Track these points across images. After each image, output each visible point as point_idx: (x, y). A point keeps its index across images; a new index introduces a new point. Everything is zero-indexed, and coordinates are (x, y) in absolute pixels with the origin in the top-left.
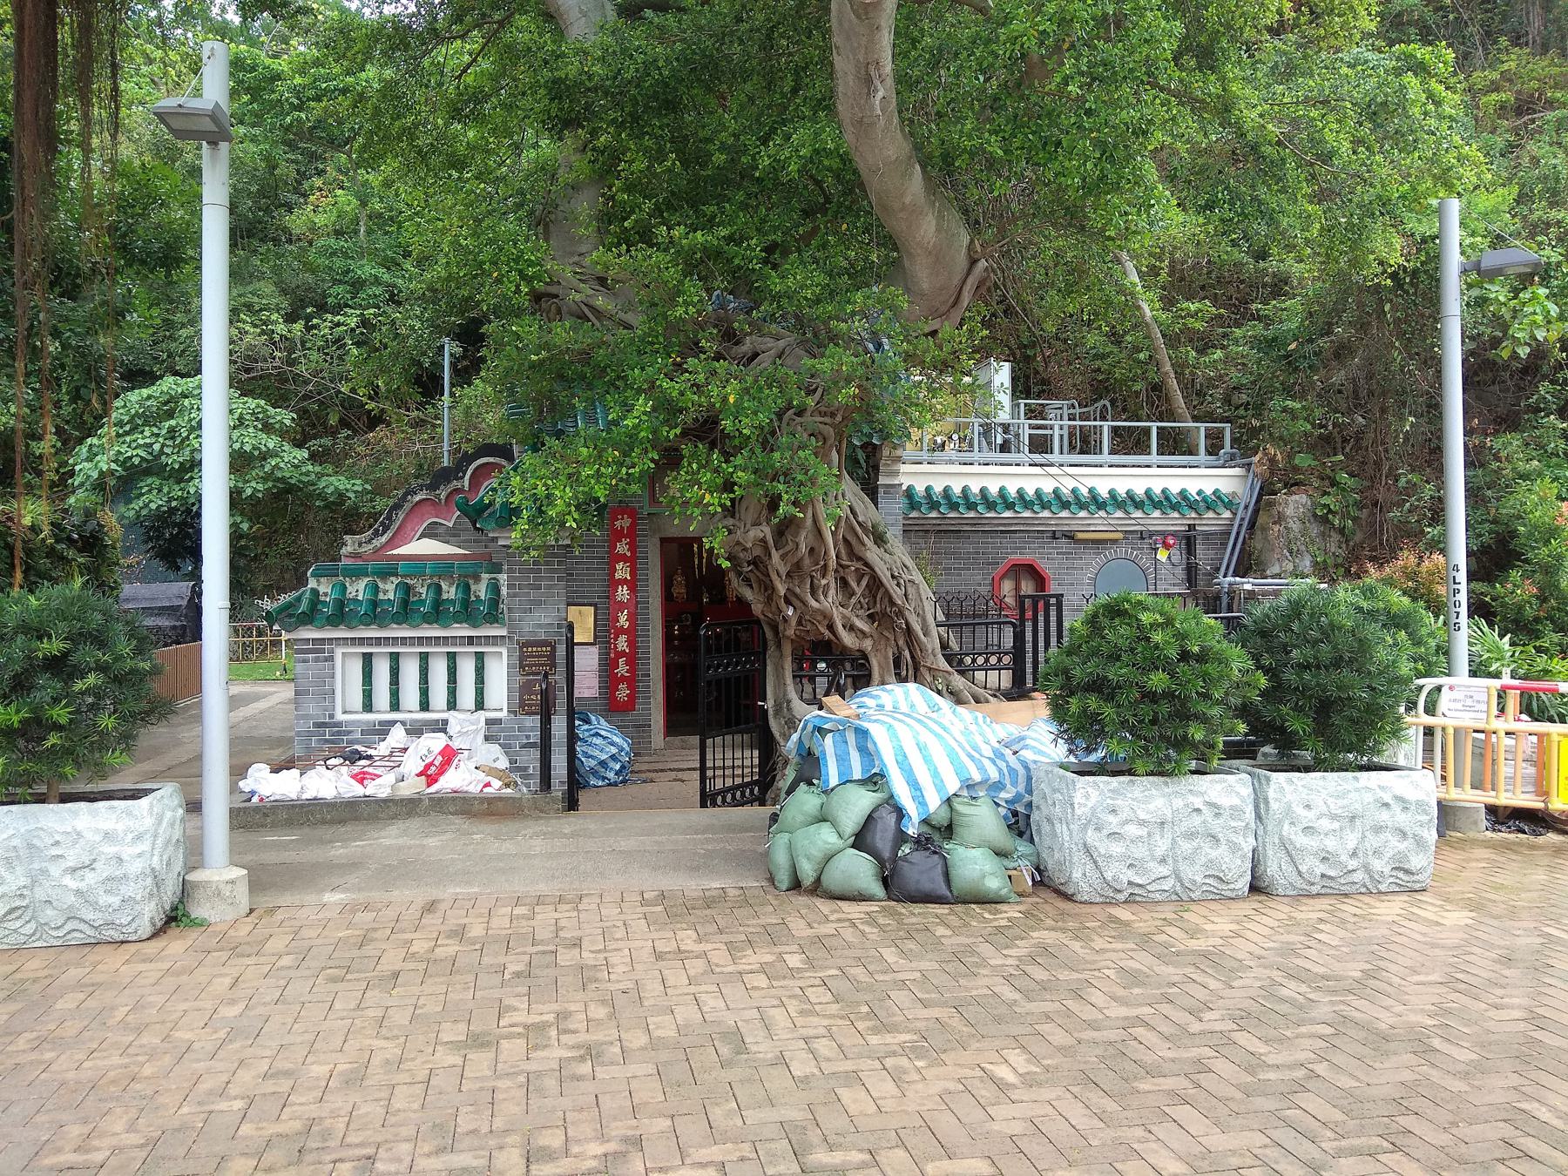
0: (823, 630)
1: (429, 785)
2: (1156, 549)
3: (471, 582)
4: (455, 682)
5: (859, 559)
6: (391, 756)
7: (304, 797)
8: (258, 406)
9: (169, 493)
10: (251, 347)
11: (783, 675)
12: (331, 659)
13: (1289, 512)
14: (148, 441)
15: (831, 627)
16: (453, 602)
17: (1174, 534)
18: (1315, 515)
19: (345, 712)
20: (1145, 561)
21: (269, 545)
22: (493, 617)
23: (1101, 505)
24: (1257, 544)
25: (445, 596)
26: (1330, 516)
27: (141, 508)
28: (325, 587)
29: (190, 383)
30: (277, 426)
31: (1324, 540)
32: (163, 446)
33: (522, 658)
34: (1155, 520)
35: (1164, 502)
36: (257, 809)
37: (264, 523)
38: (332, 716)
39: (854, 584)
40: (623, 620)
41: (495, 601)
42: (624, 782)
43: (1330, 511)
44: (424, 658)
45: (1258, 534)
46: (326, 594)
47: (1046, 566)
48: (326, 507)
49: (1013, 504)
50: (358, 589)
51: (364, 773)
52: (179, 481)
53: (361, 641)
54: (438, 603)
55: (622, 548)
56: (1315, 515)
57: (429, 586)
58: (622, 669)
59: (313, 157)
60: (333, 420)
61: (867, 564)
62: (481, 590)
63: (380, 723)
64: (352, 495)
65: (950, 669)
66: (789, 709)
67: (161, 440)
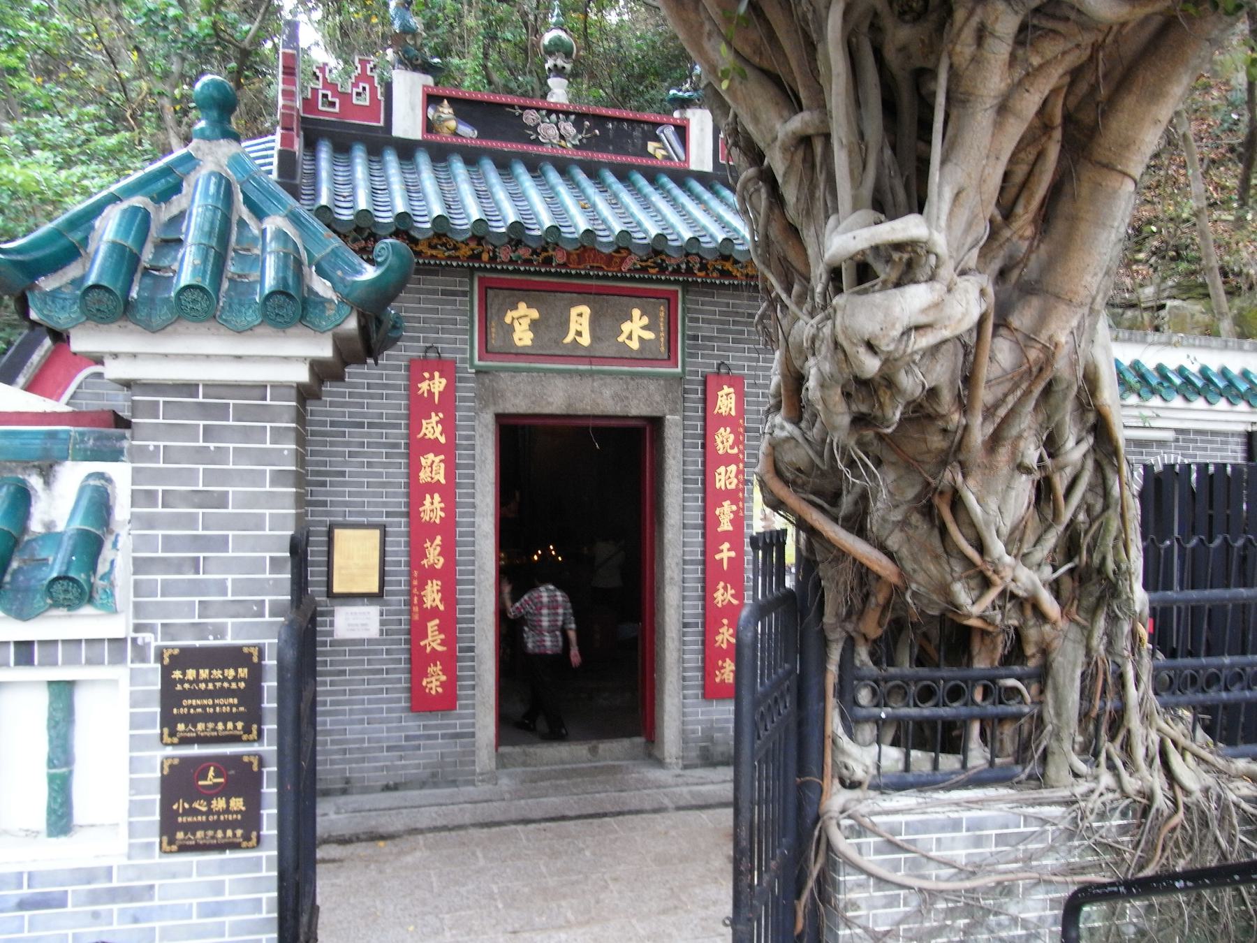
3: (35, 481)
29: (911, 703)
33: (170, 696)
55: (432, 428)
58: (434, 640)
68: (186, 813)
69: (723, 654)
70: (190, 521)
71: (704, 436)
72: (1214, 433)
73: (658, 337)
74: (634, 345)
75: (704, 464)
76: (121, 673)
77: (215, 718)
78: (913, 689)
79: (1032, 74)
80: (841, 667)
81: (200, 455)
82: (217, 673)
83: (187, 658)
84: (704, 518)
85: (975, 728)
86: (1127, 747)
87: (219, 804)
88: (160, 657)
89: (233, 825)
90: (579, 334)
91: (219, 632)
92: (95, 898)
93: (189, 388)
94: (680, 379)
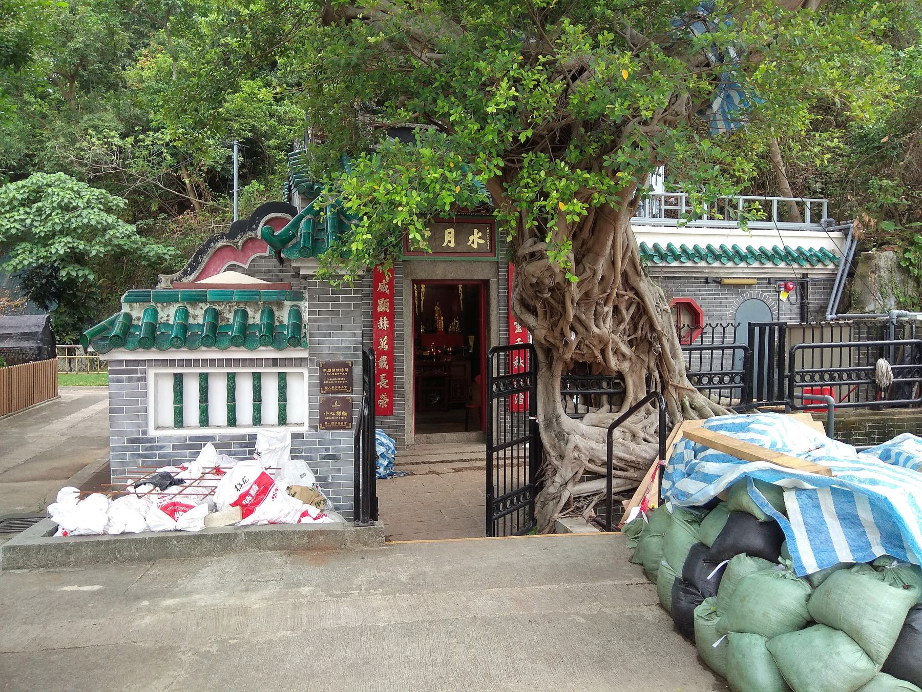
0: (597, 353)
1: (245, 515)
2: (779, 292)
3: (275, 308)
4: (260, 400)
5: (633, 289)
6: (201, 478)
7: (112, 531)
8: (101, 194)
9: (37, 253)
10: (96, 155)
11: (553, 397)
12: (144, 379)
13: (882, 263)
14: (22, 217)
15: (603, 352)
16: (258, 327)
17: (792, 280)
18: (899, 266)
19: (157, 428)
20: (772, 301)
21: (111, 293)
22: (296, 340)
23: (743, 258)
24: (857, 287)
25: (251, 321)
26: (911, 268)
27: (17, 264)
28: (138, 312)
30: (114, 208)
31: (904, 285)
32: (33, 221)
33: (322, 379)
34: (782, 270)
35: (787, 256)
36: (58, 547)
37: (107, 277)
38: (145, 433)
39: (624, 312)
40: (384, 344)
41: (298, 326)
42: (391, 475)
43: (911, 264)
44: (231, 378)
45: (858, 281)
46: (138, 319)
47: (700, 304)
48: (149, 265)
49: (680, 256)
50: (169, 314)
51: (175, 504)
52: (45, 246)
53: (173, 363)
54: (245, 328)
56: (899, 266)
57: (236, 312)
58: (383, 382)
59: (141, 35)
60: (154, 207)
61: (637, 293)
62: (284, 316)
63: (191, 439)
64: (167, 257)
65: (693, 388)
66: (558, 423)
67: (31, 216)
68: (328, 416)
74: (475, 246)
77: (338, 385)
82: (338, 370)
83: (327, 365)
87: (339, 413)
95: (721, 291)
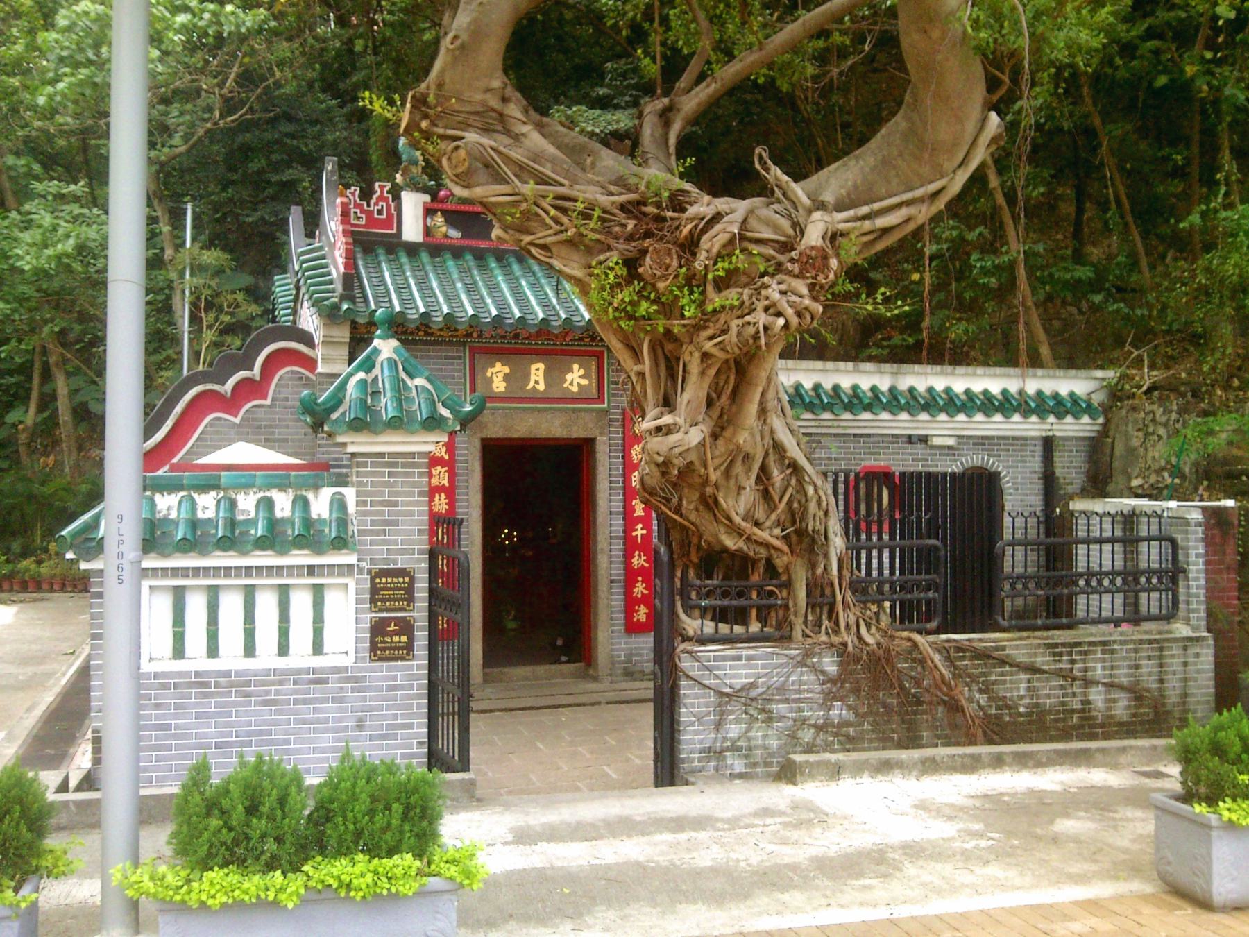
22: (341, 543)
33: (374, 590)
50: (207, 505)
69: (639, 602)
70: (381, 513)
71: (624, 451)
72: (1014, 438)
73: (590, 384)
74: (575, 389)
75: (624, 469)
76: (351, 583)
77: (395, 600)
78: (719, 591)
79: (709, 367)
80: (682, 580)
81: (387, 484)
84: (624, 507)
85: (754, 613)
86: (837, 623)
87: (396, 639)
88: (370, 572)
89: (402, 649)
90: (537, 382)
91: (395, 562)
92: (341, 680)
93: (381, 455)
94: (606, 412)
95: (931, 455)
